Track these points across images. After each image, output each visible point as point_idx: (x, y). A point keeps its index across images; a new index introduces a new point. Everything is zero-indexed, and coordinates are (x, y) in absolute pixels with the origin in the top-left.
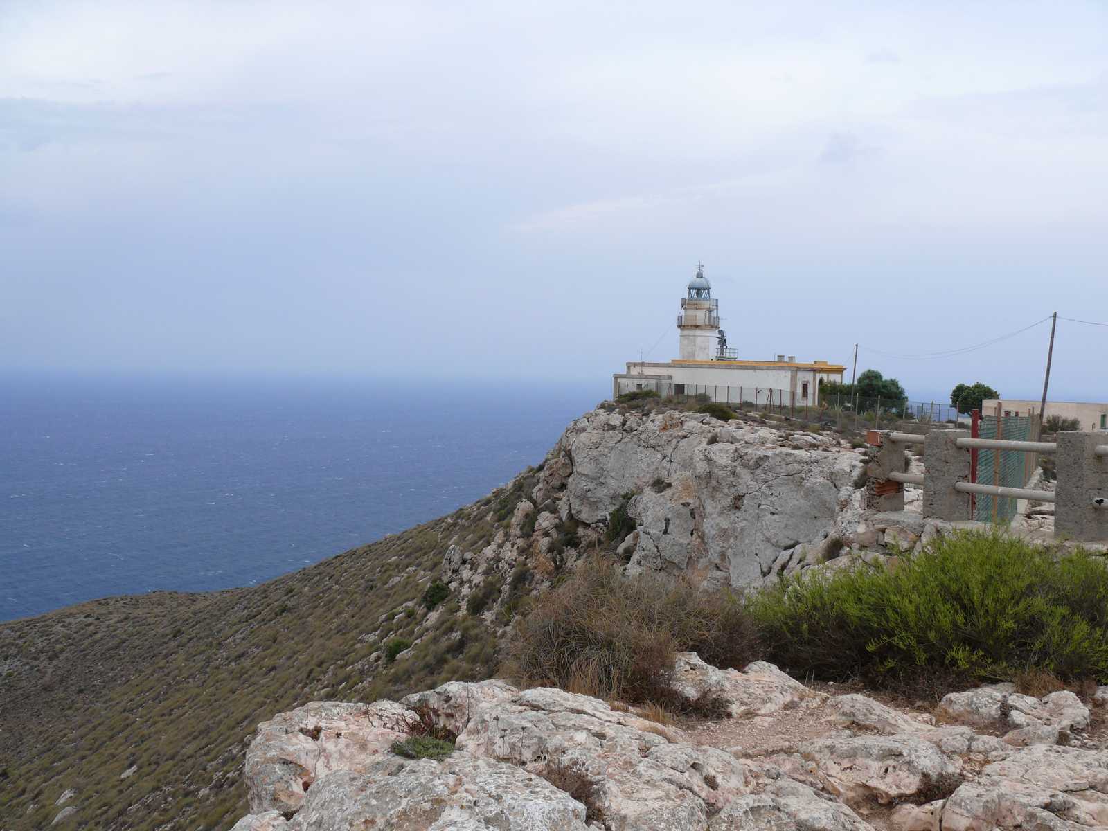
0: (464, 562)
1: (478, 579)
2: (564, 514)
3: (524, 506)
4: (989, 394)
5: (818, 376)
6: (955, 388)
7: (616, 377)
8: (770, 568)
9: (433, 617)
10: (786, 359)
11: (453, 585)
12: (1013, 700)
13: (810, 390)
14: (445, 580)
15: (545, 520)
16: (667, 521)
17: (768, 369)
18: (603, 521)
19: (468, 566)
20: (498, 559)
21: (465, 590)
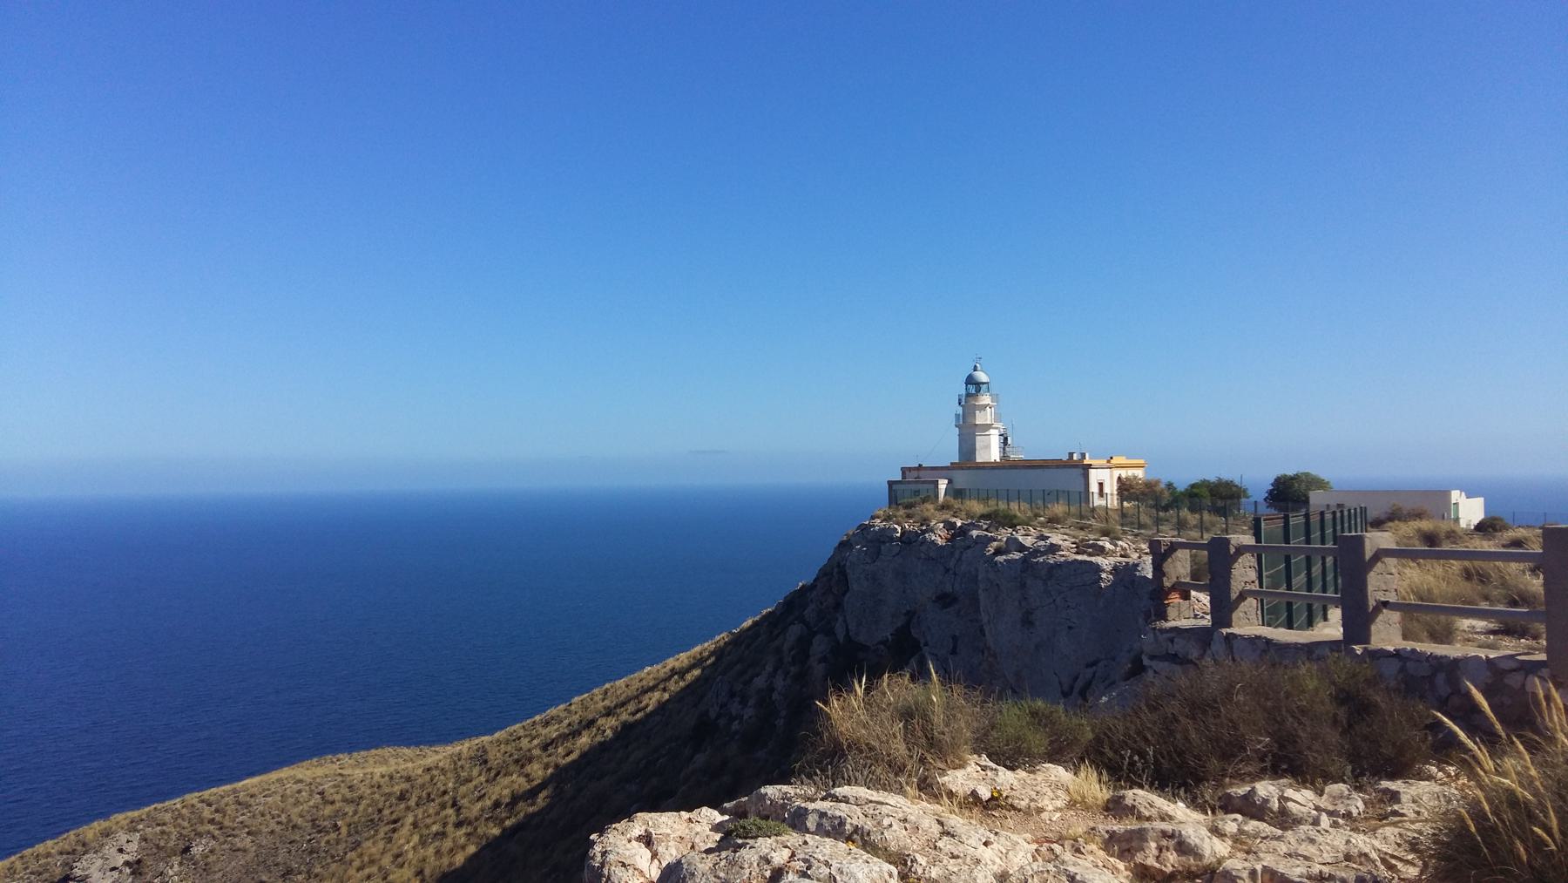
0: (732, 695)
1: (749, 712)
2: (841, 638)
3: (795, 630)
4: (1319, 484)
5: (1117, 473)
6: (1212, 478)
7: (891, 483)
8: (1072, 688)
9: (700, 759)
10: (1075, 457)
11: (722, 722)
12: (1289, 793)
13: (1107, 490)
14: (713, 715)
15: (819, 645)
16: (954, 638)
17: (1058, 467)
18: (884, 642)
19: (737, 699)
20: (771, 689)
21: (735, 726)
